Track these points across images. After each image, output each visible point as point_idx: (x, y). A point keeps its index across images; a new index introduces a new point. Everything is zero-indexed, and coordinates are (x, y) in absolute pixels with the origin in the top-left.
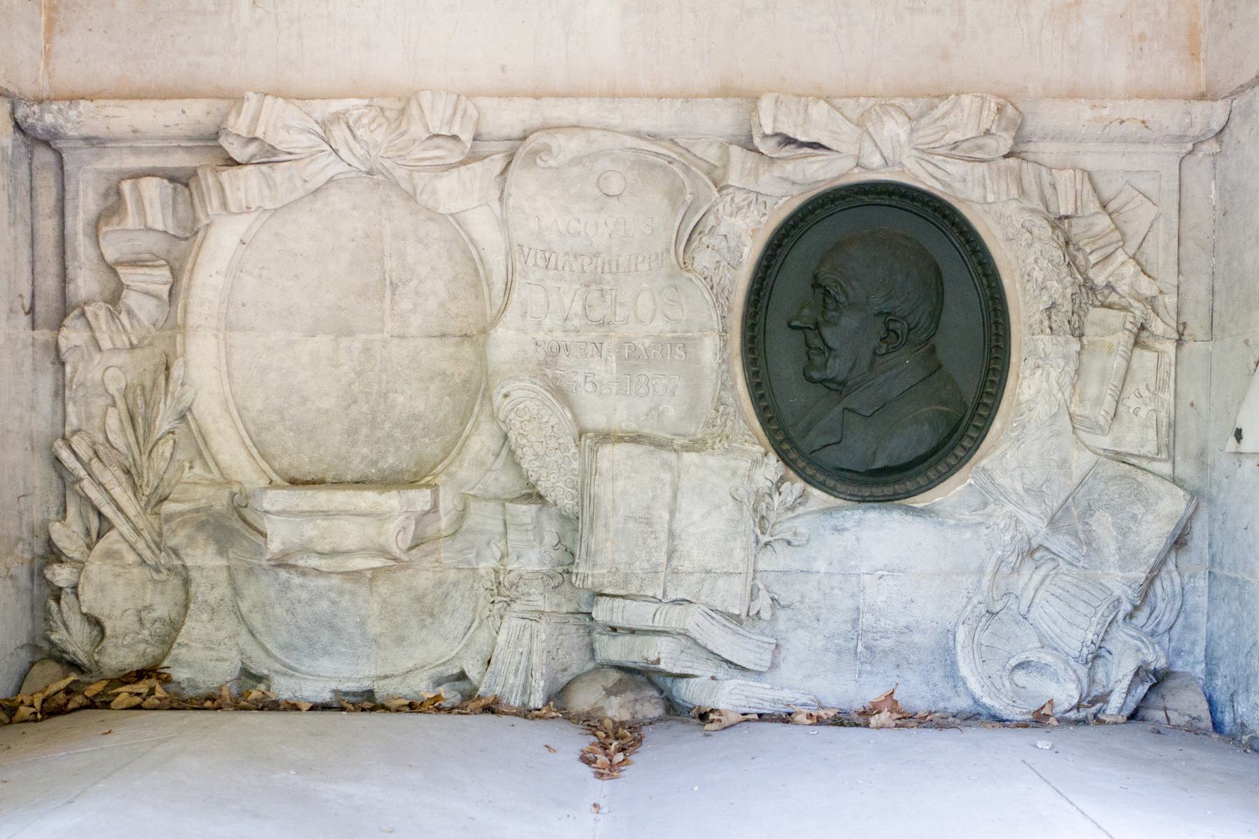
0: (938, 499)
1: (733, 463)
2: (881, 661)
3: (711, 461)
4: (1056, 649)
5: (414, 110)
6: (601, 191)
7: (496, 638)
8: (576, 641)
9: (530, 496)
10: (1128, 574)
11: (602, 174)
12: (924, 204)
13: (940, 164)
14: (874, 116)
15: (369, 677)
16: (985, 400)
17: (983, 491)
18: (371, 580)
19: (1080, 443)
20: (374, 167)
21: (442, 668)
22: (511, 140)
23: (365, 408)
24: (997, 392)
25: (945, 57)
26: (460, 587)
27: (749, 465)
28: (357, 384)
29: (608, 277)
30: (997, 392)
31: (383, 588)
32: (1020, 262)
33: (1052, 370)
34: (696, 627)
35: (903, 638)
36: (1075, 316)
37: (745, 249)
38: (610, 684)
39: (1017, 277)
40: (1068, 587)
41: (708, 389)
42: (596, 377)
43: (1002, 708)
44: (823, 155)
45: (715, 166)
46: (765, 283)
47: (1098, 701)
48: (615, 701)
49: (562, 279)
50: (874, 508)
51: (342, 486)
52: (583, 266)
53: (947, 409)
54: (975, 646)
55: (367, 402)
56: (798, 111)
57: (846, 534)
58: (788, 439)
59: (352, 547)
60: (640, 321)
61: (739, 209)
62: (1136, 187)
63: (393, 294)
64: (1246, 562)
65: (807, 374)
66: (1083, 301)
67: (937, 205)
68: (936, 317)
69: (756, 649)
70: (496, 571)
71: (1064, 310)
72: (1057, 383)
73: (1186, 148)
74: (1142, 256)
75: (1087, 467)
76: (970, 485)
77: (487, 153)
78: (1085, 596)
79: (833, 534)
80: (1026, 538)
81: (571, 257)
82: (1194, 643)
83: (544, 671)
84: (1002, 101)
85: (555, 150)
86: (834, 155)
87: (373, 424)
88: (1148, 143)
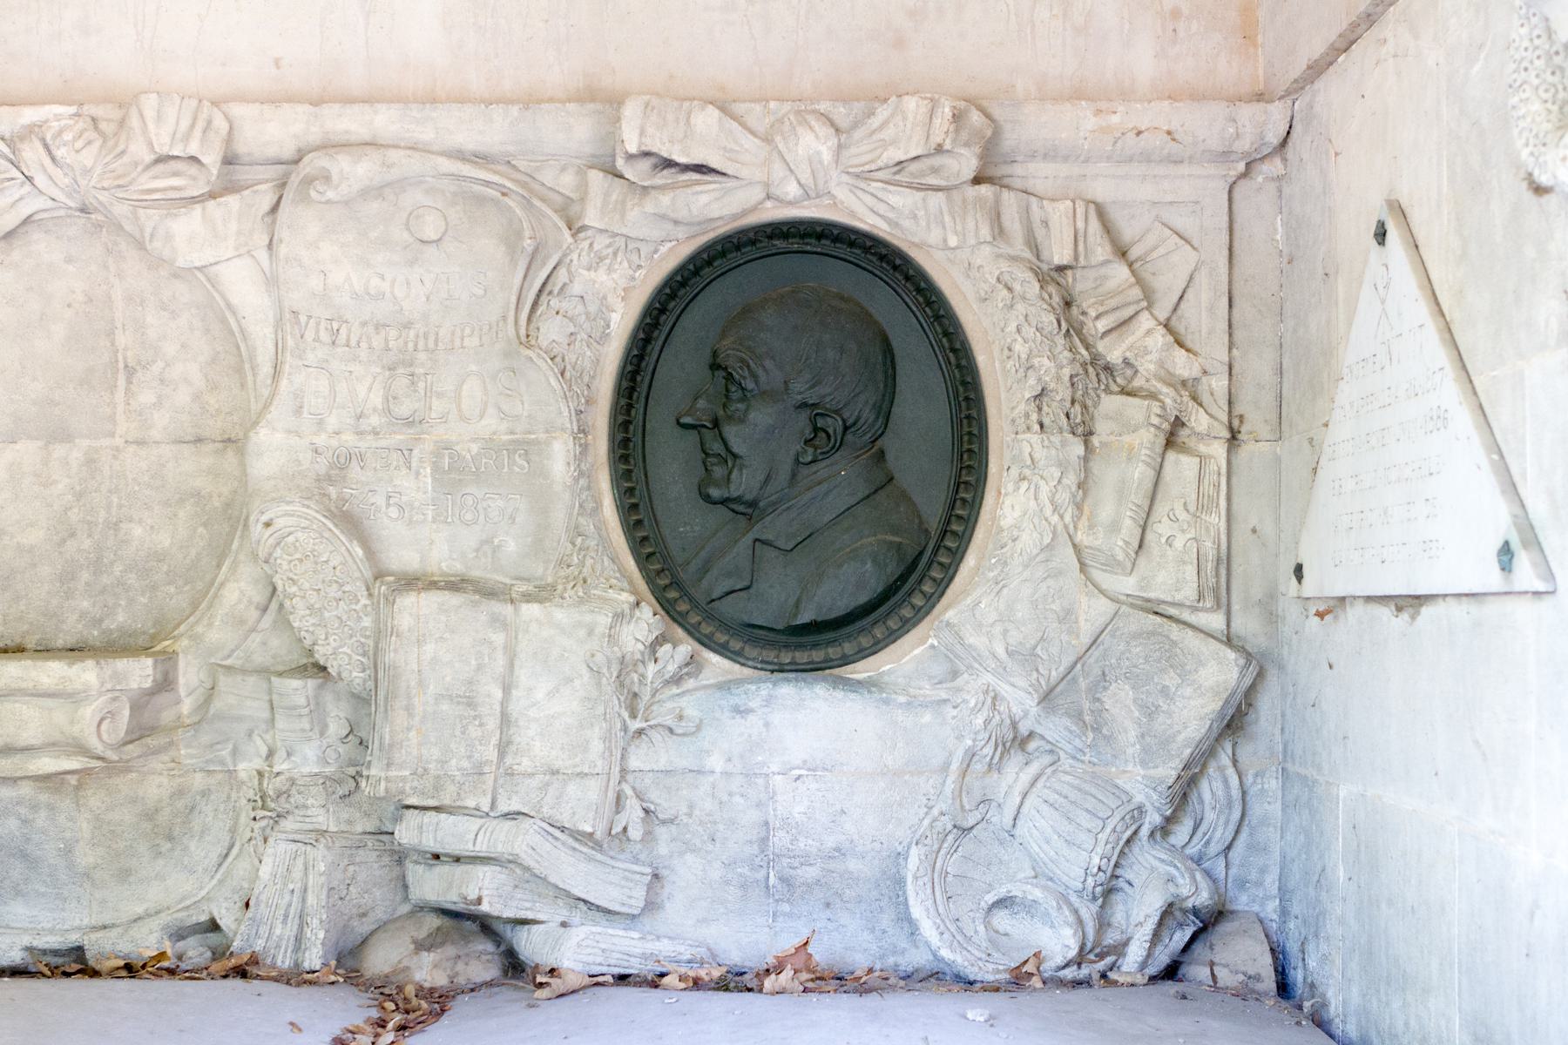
0: (888, 667)
1: (588, 618)
2: (803, 899)
3: (560, 615)
4: (1051, 879)
5: (134, 122)
6: (413, 235)
7: (258, 870)
8: (377, 873)
9: (304, 668)
10: (1152, 772)
11: (413, 211)
12: (866, 250)
13: (880, 195)
14: (786, 127)
15: (79, 928)
16: (954, 527)
17: (951, 656)
18: (78, 788)
19: (1091, 586)
20: (87, 202)
21: (184, 914)
22: (282, 163)
23: (87, 544)
24: (969, 515)
25: (900, 43)
26: (212, 797)
27: (610, 620)
28: (76, 510)
29: (422, 356)
30: (969, 515)
31: (95, 799)
32: (998, 330)
33: (1042, 483)
34: (530, 851)
35: (832, 865)
36: (1077, 407)
37: (614, 315)
38: (422, 934)
39: (996, 353)
40: (1066, 790)
41: (559, 517)
42: (404, 498)
43: (966, 964)
44: (715, 182)
45: (572, 199)
46: (644, 364)
47: (1108, 954)
48: (428, 958)
49: (355, 359)
50: (788, 680)
51: (50, 654)
52: (386, 341)
53: (897, 539)
54: (936, 875)
55: (90, 536)
56: (677, 120)
57: (751, 717)
58: (675, 583)
59: (33, 742)
60: (464, 419)
61: (601, 259)
62: (1170, 225)
63: (129, 382)
64: (1314, 754)
65: (703, 491)
66: (1090, 386)
67: (884, 251)
68: (885, 411)
69: (623, 883)
70: (260, 774)
71: (1058, 398)
72: (1052, 502)
73: (1235, 169)
74: (1180, 322)
75: (1102, 620)
76: (932, 647)
77: (250, 182)
78: (1090, 803)
79: (734, 718)
80: (1008, 721)
81: (371, 329)
82: (1263, 871)
83: (324, 917)
84: (963, 104)
85: (335, 177)
86: (731, 183)
87: (98, 566)
88: (1182, 162)
